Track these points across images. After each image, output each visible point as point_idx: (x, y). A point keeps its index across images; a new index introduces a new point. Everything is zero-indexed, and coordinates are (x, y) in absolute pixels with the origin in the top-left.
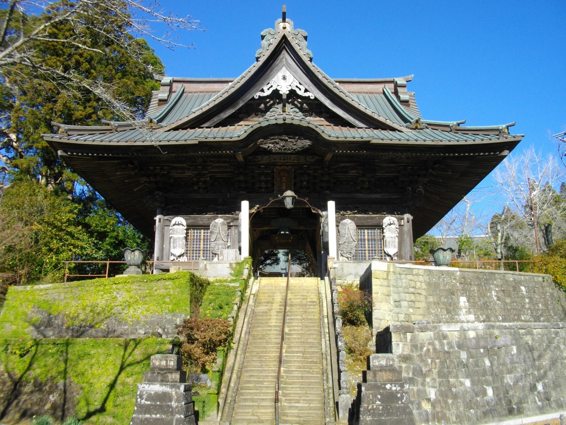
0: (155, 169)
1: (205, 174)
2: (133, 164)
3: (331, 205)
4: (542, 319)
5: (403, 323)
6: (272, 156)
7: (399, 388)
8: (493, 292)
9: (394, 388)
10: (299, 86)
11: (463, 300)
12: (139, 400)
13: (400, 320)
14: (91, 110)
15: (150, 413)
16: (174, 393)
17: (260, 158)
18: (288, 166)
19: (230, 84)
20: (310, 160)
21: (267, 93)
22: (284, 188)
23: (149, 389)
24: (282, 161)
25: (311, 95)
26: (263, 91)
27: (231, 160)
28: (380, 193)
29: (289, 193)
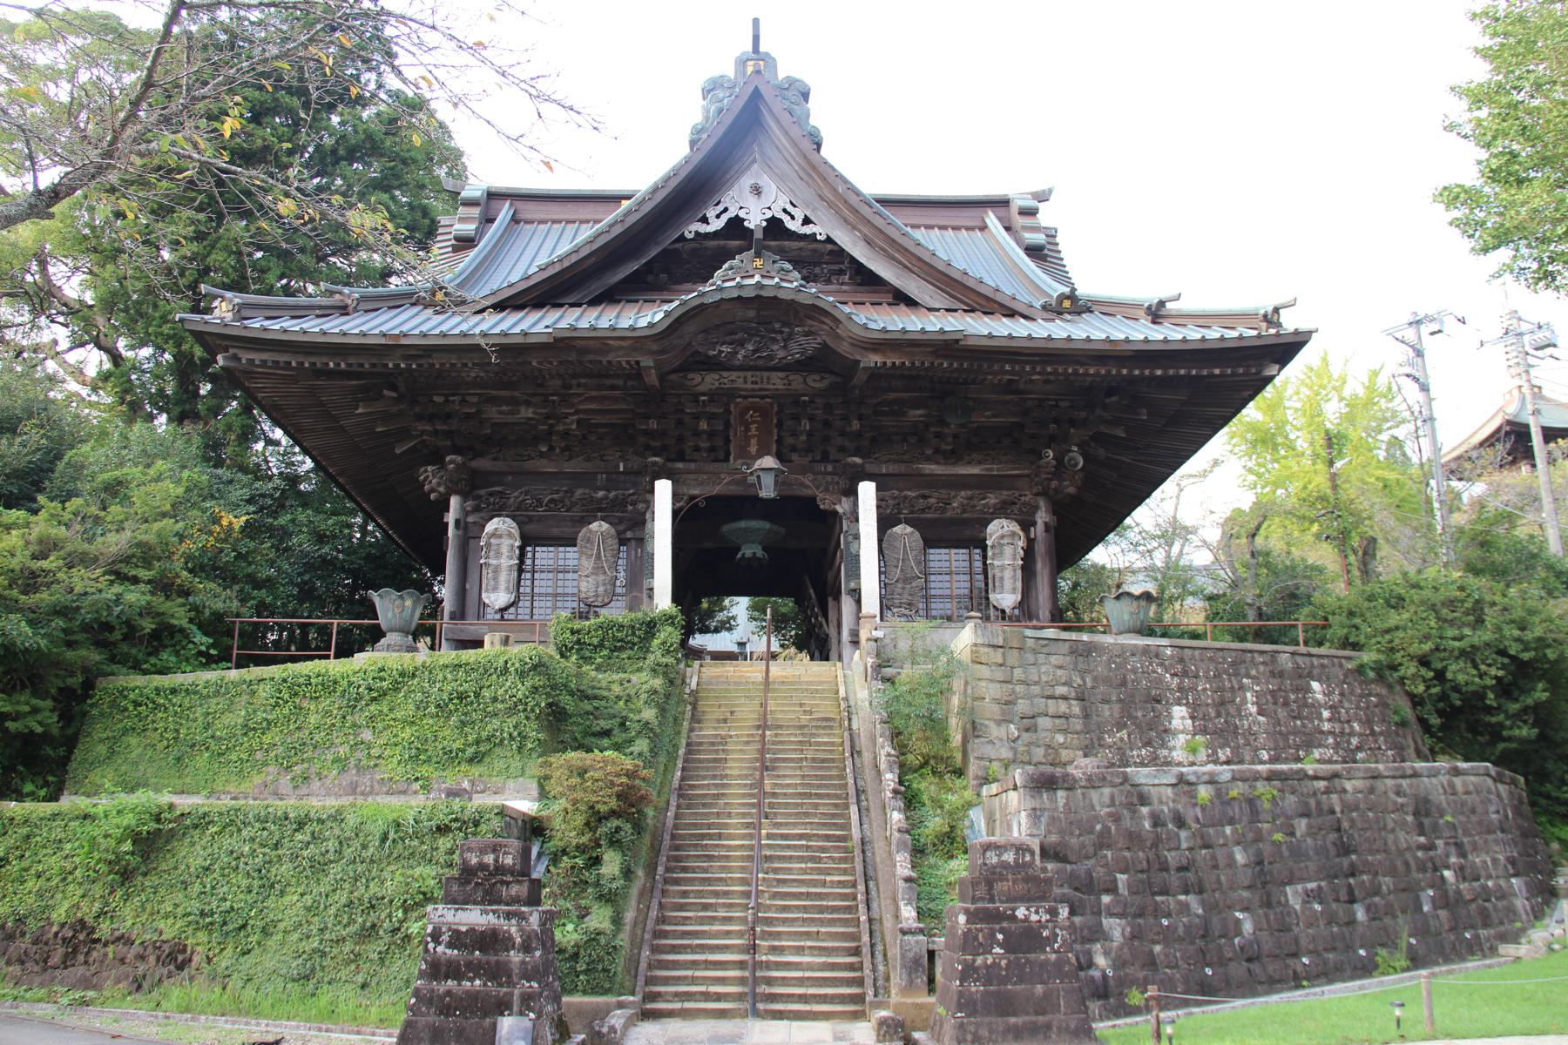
0: (447, 401)
1: (567, 415)
2: (394, 388)
3: (867, 491)
4: (1360, 756)
5: (1042, 768)
6: (725, 374)
7: (1045, 917)
8: (1249, 695)
9: (1034, 918)
10: (790, 208)
11: (1179, 716)
12: (431, 946)
13: (1035, 760)
14: (309, 254)
15: (459, 977)
16: (513, 930)
17: (698, 378)
18: (762, 397)
19: (625, 204)
20: (817, 385)
21: (716, 225)
22: (753, 449)
23: (457, 920)
24: (750, 386)
25: (819, 230)
26: (705, 220)
27: (630, 383)
28: (980, 463)
29: (769, 462)
